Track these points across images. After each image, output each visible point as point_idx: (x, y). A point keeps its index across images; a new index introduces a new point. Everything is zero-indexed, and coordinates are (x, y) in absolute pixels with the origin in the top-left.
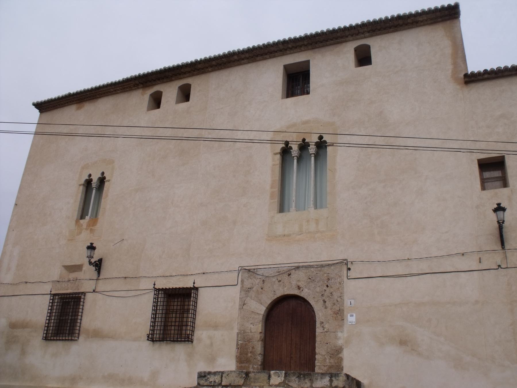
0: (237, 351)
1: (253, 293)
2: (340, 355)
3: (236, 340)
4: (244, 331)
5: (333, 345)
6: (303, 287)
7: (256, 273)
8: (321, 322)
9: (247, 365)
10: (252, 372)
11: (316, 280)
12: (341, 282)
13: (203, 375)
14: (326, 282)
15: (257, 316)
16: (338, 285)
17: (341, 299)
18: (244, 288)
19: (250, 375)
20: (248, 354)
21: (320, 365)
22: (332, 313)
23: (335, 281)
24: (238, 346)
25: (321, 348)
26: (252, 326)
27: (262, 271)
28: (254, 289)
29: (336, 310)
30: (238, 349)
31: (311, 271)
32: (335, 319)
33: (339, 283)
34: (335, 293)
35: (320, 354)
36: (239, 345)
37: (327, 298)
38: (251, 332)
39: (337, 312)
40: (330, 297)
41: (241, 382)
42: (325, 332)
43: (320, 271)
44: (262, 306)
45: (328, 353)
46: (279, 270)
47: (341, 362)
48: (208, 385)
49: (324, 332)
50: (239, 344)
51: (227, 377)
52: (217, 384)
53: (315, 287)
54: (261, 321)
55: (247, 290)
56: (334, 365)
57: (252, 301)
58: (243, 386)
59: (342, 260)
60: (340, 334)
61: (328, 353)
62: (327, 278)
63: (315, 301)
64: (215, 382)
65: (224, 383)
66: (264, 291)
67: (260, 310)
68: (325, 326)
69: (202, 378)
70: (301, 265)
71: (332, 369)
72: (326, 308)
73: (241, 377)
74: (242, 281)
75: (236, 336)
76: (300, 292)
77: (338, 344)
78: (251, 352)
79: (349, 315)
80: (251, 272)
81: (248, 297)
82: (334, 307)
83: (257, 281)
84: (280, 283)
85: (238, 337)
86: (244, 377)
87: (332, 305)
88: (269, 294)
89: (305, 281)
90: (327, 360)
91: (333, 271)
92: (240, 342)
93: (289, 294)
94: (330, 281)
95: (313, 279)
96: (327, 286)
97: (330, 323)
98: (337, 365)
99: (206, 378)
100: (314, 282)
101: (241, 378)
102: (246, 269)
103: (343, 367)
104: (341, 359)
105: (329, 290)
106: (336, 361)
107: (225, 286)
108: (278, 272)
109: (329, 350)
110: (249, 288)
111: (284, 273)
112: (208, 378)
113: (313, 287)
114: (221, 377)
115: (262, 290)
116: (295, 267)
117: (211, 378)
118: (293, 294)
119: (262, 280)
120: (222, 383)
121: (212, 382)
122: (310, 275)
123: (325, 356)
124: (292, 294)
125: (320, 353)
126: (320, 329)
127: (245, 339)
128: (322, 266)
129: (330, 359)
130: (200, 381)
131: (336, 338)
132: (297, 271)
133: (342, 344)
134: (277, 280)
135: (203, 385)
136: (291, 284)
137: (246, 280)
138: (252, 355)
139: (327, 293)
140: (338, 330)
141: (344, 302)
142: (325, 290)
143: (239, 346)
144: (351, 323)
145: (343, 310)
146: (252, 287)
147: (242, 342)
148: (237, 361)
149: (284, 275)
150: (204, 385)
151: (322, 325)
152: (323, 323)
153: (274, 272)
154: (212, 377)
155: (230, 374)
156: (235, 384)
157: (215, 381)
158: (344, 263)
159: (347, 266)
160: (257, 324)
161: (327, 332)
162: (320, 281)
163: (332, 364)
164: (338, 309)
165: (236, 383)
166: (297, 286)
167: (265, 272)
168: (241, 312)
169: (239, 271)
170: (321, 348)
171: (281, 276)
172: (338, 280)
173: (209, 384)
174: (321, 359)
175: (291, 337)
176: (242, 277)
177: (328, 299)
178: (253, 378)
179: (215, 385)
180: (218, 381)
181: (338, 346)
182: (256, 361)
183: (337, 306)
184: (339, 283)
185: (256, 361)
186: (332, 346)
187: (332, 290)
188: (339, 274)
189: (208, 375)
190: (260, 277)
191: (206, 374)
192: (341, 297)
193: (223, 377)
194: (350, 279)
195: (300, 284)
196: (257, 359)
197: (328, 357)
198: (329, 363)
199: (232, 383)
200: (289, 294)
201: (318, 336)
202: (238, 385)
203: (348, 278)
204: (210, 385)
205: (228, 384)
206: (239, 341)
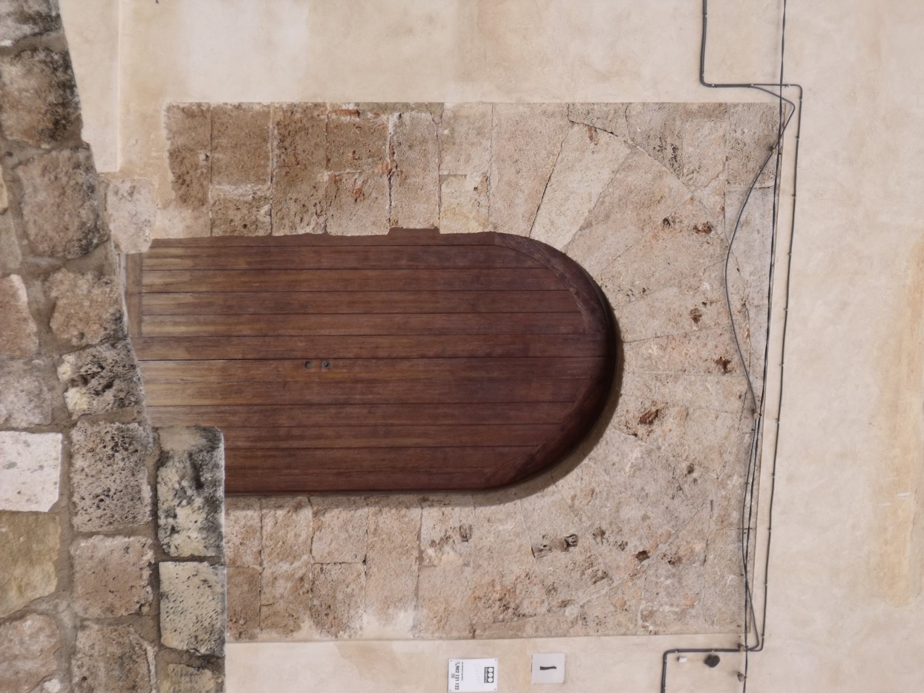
0: (344, 107)
1: (650, 176)
2: (307, 624)
3: (404, 100)
4: (451, 139)
5: (356, 592)
6: (653, 436)
7: (757, 185)
8: (471, 528)
9: (272, 165)
10: (220, 681)
11: (677, 501)
12: (655, 624)
13: (203, 479)
14: (663, 548)
15: (522, 207)
16: (642, 607)
17: (573, 623)
18: (678, 123)
19: (208, 673)
20: (327, 168)
21: (264, 533)
22: (509, 581)
23: (663, 594)
24: (371, 111)
25: (343, 536)
26: (474, 180)
27: (763, 216)
28: (671, 181)
29: (521, 602)
30: (358, 113)
31: (730, 476)
32: (477, 594)
33: (652, 614)
34: (604, 592)
35: (318, 533)
36: (377, 115)
37: (583, 558)
38: (441, 179)
39: (512, 605)
40: (590, 571)
41: (173, 640)
42: (421, 552)
43: (723, 520)
44: (574, 231)
45: (322, 569)
46: (752, 314)
47: (274, 626)
48: (160, 505)
49: (419, 546)
50: (384, 117)
51: (197, 581)
52: (166, 541)
53: (642, 496)
54: (495, 228)
55: (669, 140)
56: (263, 597)
57: (606, 175)
58: (156, 648)
59: (760, 631)
60: (405, 618)
61: (322, 569)
62: (681, 553)
63: (573, 498)
64: (174, 530)
65: (167, 568)
66: (655, 237)
67: (552, 223)
68: (447, 548)
69: (189, 471)
70: (768, 424)
71: (246, 587)
72: (538, 551)
73: (196, 637)
74: (720, 111)
75: (426, 99)
76: (627, 425)
77: (360, 611)
78: (336, 181)
79: (491, 662)
80: (764, 154)
81: (628, 151)
82: (538, 592)
83: (710, 199)
84: (687, 322)
85: (420, 107)
86: (198, 651)
87: (549, 582)
88: (635, 265)
89: (682, 445)
90: (285, 567)
91: (715, 584)
92: (390, 121)
93: (622, 369)
94: (665, 568)
95: (686, 487)
96: (643, 555)
97: (462, 572)
98: (264, 609)
99: (189, 492)
100: (670, 492)
101: (193, 639)
102: (783, 126)
103: (252, 638)
104: (291, 628)
105: (622, 564)
106: (281, 606)
107: (704, 13)
108: (744, 305)
109: (335, 572)
110: (679, 152)
111: (735, 340)
112: (190, 501)
113: (647, 488)
114: (196, 554)
115: (660, 221)
116: (759, 393)
117: (190, 511)
118: (623, 392)
119: (712, 221)
120: (170, 563)
121: (171, 520)
122: (707, 469)
123: (305, 557)
124: (624, 384)
125: (319, 528)
126: (438, 528)
127: (405, 148)
128: (745, 532)
129: (289, 577)
130: (178, 465)
131: (388, 604)
132: (736, 404)
133: (361, 628)
134: (704, 304)
135: (157, 483)
136: (676, 378)
137: (721, 133)
138: (321, 192)
139: (606, 555)
140: (425, 611)
141: (557, 636)
142: (623, 546)
143: (370, 115)
144: (452, 670)
145: (516, 634)
146: (681, 167)
147: (391, 129)
148: (292, 109)
149: (727, 336)
150: (159, 486)
151: (457, 537)
152: (465, 538)
153: (746, 284)
154: (194, 517)
155: (208, 591)
156: (163, 615)
157: (178, 532)
158: (746, 633)
159: (727, 647)
160: (484, 211)
161: (420, 559)
162: (673, 523)
163: (266, 590)
164: (526, 608)
165: (166, 622)
166: (660, 406)
167: (755, 235)
168: (553, 115)
169: (777, 90)
170: (343, 536)
171: (725, 321)
172: (667, 608)
173: (163, 507)
174: (291, 535)
175: (408, 358)
176: (740, 108)
177: (580, 558)
178: (192, 688)
179: (161, 534)
180: (177, 543)
181: (352, 612)
182: (292, 213)
183: (543, 601)
184: (652, 614)
185: (292, 213)
186: (352, 586)
187: (619, 577)
188: (693, 612)
189: (205, 498)
190: (731, 212)
191: (207, 491)
192: (580, 622)
193: (195, 564)
194: (664, 663)
195: (669, 423)
196: (302, 220)
197: (300, 568)
198: (273, 573)
199: (171, 605)
200: (627, 367)
201: (404, 516)
202: (163, 632)
203: (670, 657)
204: (160, 513)
205: (165, 587)
206: (396, 114)
